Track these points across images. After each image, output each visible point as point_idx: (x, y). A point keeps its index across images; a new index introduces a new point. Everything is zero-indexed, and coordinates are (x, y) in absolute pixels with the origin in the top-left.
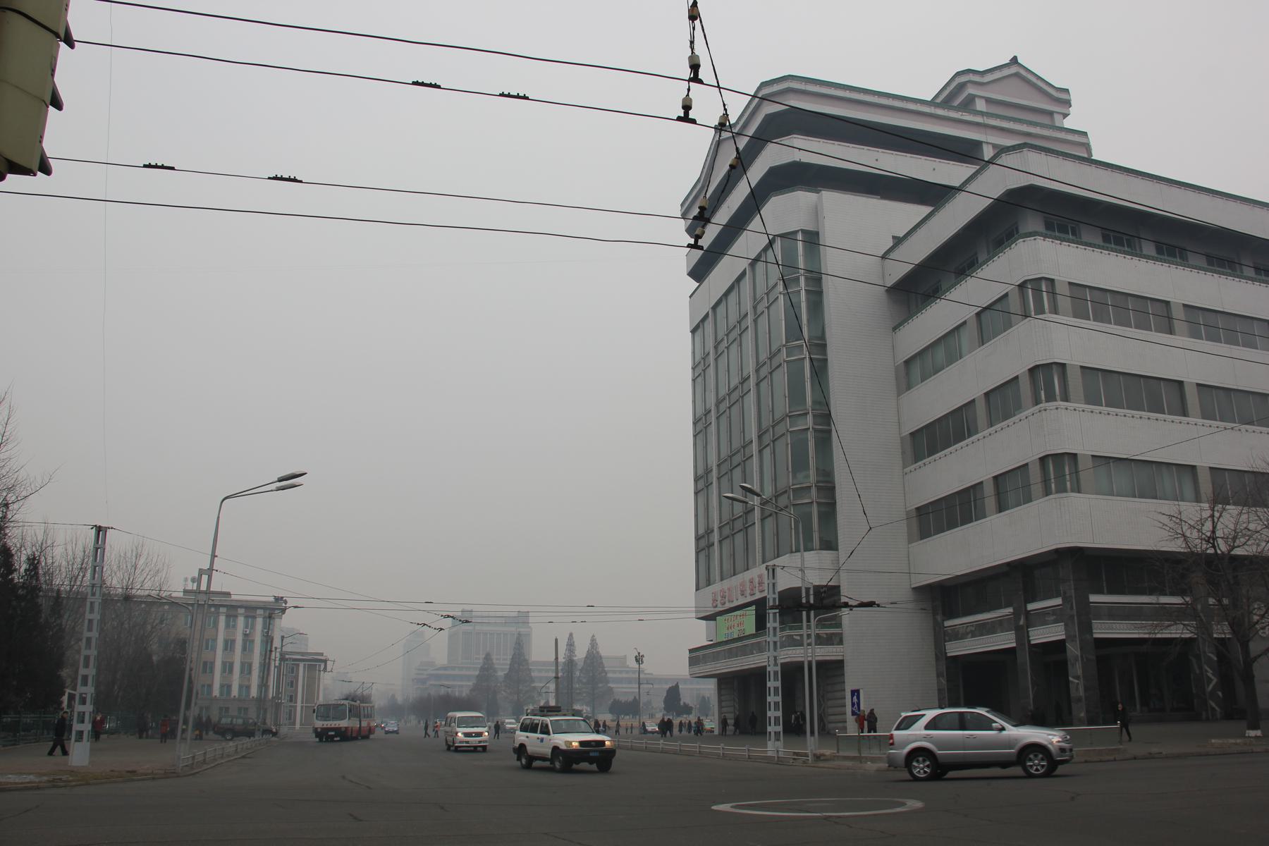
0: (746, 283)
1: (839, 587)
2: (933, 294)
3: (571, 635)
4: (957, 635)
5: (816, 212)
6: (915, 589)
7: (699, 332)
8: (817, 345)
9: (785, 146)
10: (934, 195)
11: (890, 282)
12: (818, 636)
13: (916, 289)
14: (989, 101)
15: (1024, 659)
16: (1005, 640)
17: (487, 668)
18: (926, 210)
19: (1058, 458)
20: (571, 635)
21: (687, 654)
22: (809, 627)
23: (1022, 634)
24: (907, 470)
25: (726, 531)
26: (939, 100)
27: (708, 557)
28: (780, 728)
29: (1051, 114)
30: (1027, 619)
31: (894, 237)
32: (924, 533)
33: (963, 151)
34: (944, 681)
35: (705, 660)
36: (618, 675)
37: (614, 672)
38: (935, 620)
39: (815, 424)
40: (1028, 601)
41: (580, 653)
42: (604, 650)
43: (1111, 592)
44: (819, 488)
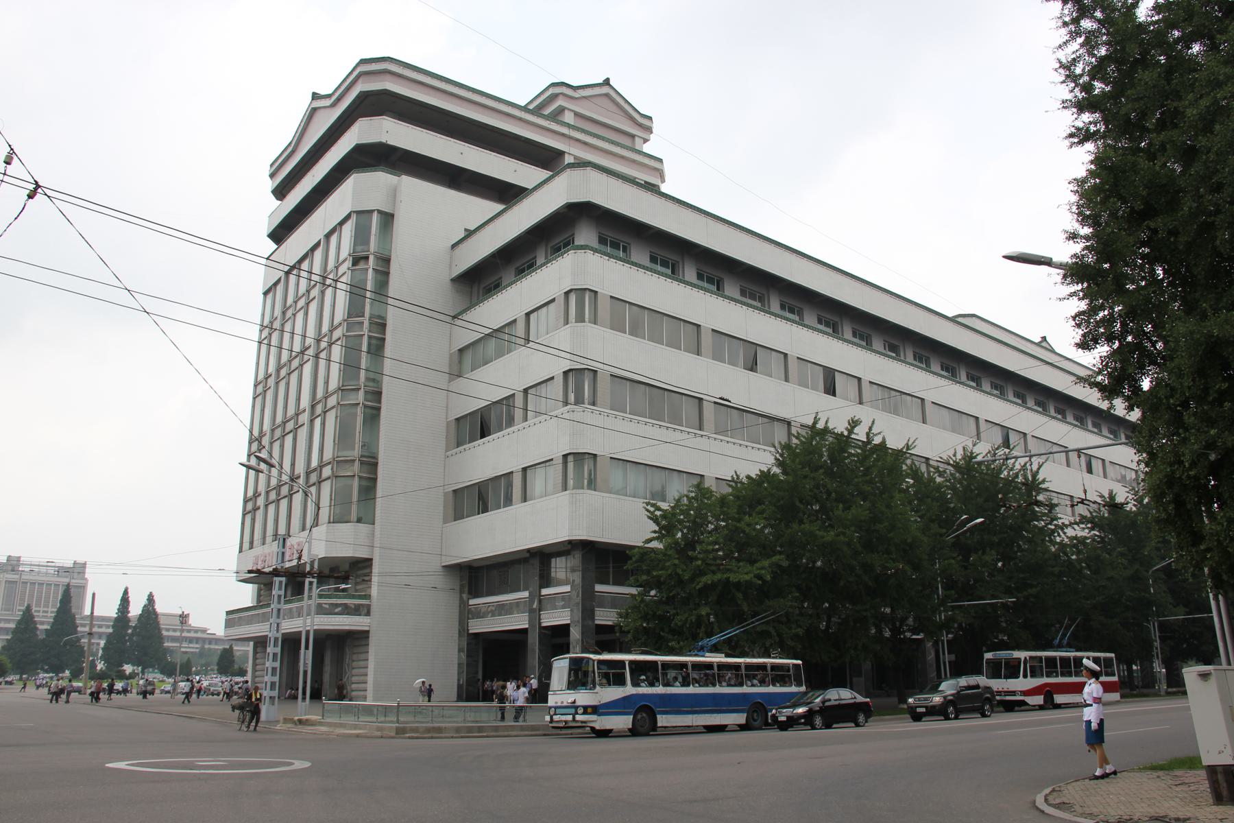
0: (318, 254)
1: (371, 560)
2: (494, 288)
3: (126, 592)
4: (478, 614)
5: (394, 194)
6: (445, 567)
7: (270, 296)
8: (377, 324)
9: (385, 125)
10: (507, 194)
11: (455, 274)
12: (320, 605)
13: (481, 280)
14: (577, 114)
15: (534, 640)
16: (518, 622)
17: (27, 619)
18: (500, 207)
19: (579, 457)
20: (126, 592)
21: (224, 616)
22: (310, 597)
23: (535, 614)
24: (449, 453)
25: (273, 496)
26: (531, 107)
27: (253, 520)
28: (275, 693)
29: (633, 136)
30: (540, 601)
31: (466, 230)
32: (459, 515)
33: (548, 159)
34: (464, 656)
35: (240, 622)
36: (171, 633)
37: (168, 630)
38: (461, 598)
39: (366, 400)
40: (542, 586)
41: (135, 610)
42: (160, 608)
43: (616, 583)
44: (362, 463)
